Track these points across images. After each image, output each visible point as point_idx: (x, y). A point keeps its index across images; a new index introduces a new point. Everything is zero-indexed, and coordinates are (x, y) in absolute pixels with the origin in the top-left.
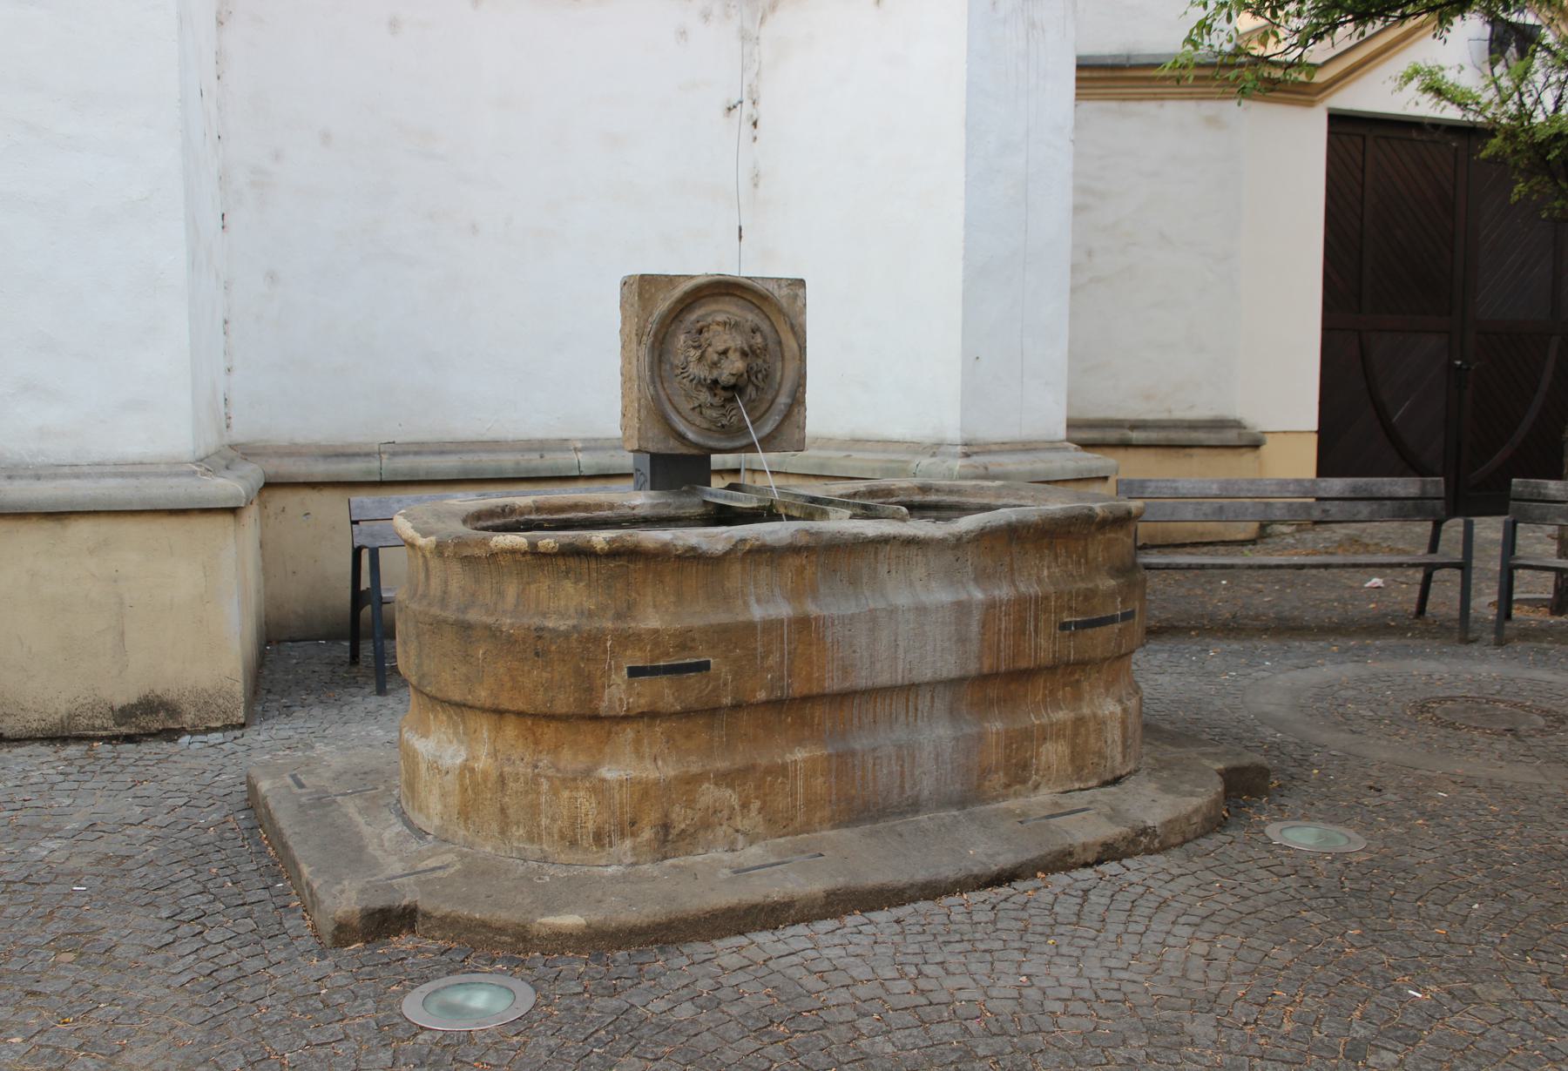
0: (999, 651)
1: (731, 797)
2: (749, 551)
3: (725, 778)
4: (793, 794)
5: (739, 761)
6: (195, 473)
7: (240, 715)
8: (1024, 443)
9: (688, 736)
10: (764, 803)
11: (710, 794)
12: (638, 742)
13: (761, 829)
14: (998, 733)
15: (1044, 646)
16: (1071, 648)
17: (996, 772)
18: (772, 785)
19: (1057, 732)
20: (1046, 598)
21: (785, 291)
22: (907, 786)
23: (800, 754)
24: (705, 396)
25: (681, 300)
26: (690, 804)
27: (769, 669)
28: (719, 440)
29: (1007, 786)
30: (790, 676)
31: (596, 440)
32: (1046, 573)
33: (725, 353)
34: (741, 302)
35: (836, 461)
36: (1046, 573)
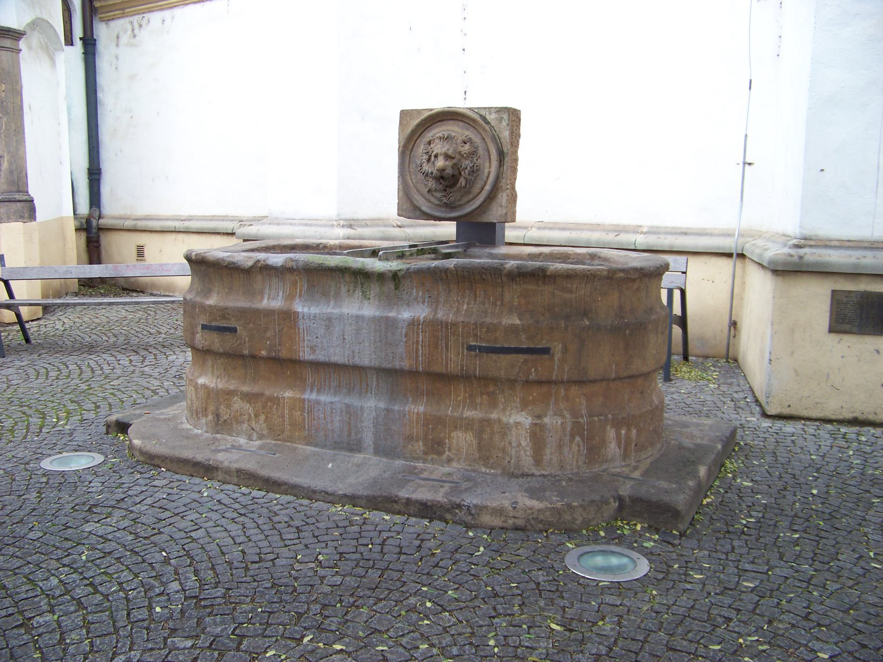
0: (417, 356)
1: (248, 408)
2: (261, 268)
3: (248, 397)
4: (283, 417)
5: (256, 389)
6: (333, 225)
7: (40, 315)
8: (872, 243)
9: (234, 369)
10: (267, 417)
11: (238, 404)
12: (213, 367)
13: (265, 432)
14: (418, 414)
15: (454, 360)
16: (479, 365)
17: (417, 441)
18: (271, 408)
19: (468, 425)
20: (454, 325)
21: (493, 116)
22: (353, 434)
23: (288, 394)
24: (432, 184)
25: (419, 125)
26: (229, 406)
27: (268, 339)
28: (446, 212)
29: (425, 453)
30: (280, 345)
31: (658, 227)
32: (465, 307)
33: (436, 156)
34: (461, 124)
35: (534, 234)
36: (465, 307)
